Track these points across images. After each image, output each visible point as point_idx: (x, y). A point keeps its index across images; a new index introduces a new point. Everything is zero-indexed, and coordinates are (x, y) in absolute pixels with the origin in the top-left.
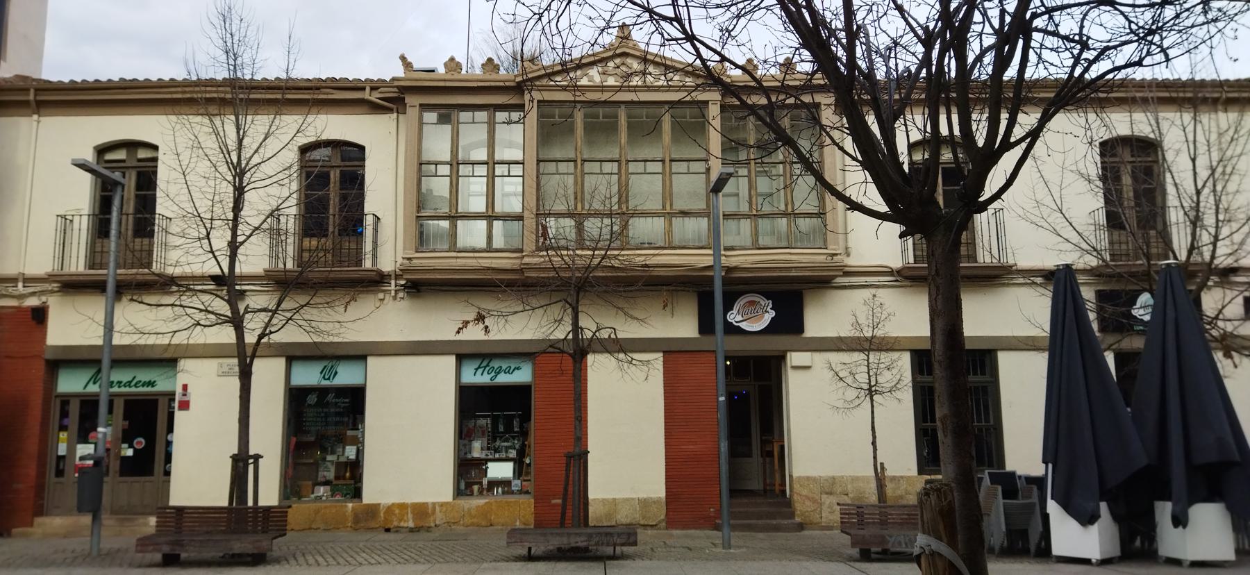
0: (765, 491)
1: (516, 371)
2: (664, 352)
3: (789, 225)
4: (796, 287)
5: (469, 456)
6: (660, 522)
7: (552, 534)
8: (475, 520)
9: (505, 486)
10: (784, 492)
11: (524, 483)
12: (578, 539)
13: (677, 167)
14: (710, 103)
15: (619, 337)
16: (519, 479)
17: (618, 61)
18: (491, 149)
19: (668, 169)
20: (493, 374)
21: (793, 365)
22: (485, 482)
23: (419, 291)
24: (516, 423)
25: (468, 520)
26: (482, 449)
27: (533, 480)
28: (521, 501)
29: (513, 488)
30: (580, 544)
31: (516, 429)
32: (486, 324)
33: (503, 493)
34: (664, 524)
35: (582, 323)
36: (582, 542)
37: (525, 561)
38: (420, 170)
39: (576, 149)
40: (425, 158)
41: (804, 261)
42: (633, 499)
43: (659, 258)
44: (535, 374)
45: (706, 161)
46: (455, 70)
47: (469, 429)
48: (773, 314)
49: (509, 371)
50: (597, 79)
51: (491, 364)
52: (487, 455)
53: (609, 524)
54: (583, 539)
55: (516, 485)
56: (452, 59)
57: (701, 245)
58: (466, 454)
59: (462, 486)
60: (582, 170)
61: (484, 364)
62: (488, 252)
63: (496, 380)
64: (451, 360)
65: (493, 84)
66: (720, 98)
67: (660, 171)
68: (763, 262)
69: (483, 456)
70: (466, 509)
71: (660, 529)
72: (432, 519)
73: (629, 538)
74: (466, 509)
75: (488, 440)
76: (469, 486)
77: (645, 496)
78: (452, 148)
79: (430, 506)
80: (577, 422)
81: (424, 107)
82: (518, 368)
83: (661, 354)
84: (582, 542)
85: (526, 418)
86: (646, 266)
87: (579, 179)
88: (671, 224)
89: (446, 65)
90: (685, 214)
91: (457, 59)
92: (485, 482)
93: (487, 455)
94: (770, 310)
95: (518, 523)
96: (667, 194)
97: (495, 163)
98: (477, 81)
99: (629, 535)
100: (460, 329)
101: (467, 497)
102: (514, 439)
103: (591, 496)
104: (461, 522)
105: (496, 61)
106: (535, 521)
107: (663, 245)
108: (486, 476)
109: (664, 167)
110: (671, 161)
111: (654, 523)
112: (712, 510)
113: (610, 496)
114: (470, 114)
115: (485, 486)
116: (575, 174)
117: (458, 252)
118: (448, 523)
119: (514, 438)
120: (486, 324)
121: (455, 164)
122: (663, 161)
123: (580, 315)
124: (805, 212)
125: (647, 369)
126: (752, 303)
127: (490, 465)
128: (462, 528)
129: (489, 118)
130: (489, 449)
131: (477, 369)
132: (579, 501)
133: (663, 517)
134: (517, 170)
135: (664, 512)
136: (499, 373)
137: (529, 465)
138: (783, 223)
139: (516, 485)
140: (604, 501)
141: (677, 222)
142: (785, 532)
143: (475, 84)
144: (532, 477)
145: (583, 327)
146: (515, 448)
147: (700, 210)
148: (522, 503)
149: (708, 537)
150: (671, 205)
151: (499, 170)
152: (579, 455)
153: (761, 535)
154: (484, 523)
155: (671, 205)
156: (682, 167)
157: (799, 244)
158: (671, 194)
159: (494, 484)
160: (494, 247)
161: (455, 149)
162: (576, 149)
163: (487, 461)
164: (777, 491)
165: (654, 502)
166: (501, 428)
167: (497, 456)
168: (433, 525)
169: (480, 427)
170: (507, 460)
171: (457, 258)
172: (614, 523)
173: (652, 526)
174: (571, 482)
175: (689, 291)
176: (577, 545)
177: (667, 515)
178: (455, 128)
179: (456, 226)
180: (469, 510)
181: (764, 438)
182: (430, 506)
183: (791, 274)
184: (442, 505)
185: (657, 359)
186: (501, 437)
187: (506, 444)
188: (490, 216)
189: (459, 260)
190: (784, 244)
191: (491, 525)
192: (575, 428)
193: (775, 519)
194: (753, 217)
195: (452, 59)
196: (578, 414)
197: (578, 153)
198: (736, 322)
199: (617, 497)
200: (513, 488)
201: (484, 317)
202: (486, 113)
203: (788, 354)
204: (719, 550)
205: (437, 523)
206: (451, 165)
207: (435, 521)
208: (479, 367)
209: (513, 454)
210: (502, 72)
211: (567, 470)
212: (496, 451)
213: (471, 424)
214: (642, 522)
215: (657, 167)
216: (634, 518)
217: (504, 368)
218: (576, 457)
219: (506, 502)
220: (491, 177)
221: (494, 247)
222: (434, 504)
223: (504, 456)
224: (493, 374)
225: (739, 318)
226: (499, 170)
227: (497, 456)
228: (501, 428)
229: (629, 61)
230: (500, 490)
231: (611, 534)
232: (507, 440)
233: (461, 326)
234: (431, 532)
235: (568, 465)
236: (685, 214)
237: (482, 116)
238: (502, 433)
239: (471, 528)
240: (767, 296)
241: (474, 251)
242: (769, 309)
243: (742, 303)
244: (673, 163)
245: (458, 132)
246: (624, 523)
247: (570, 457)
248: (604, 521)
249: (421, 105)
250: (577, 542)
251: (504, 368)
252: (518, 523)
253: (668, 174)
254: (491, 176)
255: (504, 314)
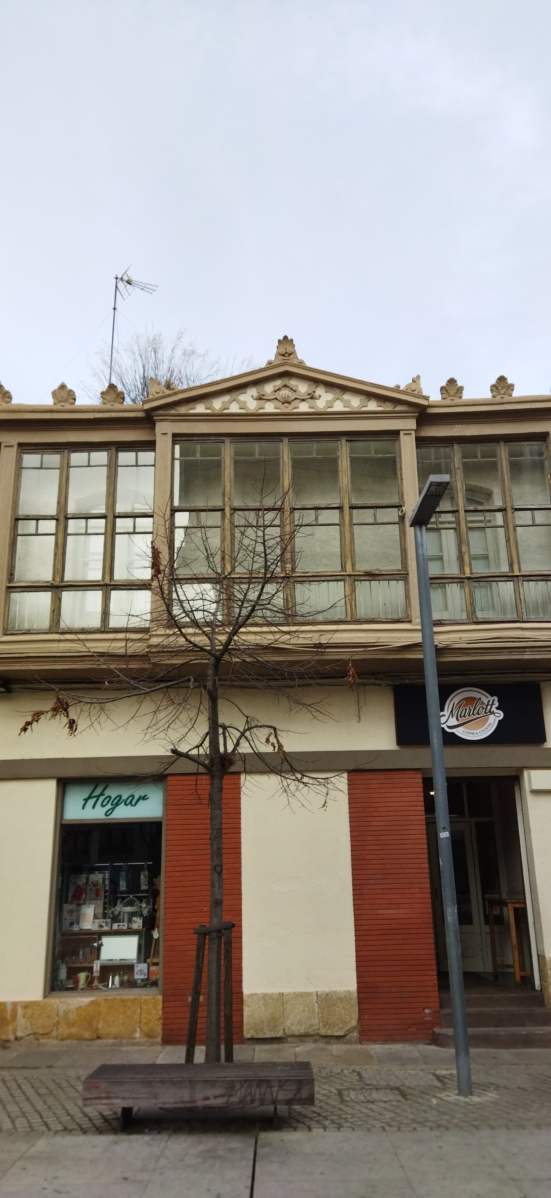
0: (496, 975)
1: (141, 801)
2: (350, 772)
3: (517, 591)
4: (529, 677)
5: (76, 928)
6: (350, 1031)
7: (162, 1082)
8: (74, 1030)
9: (124, 974)
10: (528, 980)
11: (153, 968)
12: (211, 1092)
13: (359, 516)
14: (402, 433)
15: (287, 749)
16: (145, 962)
17: (278, 383)
18: (111, 498)
19: (347, 518)
20: (109, 806)
21: (535, 787)
22: (96, 966)
23: (9, 691)
24: (143, 878)
25: (64, 1030)
26: (95, 917)
27: (161, 964)
28: (144, 997)
29: (137, 977)
30: (213, 1102)
31: (144, 887)
32: (72, 716)
33: (122, 984)
34: (356, 1034)
35: (222, 719)
36: (216, 1097)
37: (115, 1131)
38: (15, 527)
39: (224, 495)
40: (23, 511)
41: (542, 638)
42: (309, 994)
43: (337, 635)
44: (167, 805)
45: (399, 507)
46: (66, 401)
47: (79, 886)
48: (501, 715)
49: (131, 802)
50: (252, 405)
51: (107, 793)
52: (101, 926)
53: (273, 1035)
54: (217, 1092)
55: (141, 971)
56: (63, 387)
57: (395, 617)
58: (72, 924)
59: (63, 974)
60: (232, 523)
61: (97, 792)
62: (103, 632)
63: (112, 816)
64: (50, 787)
65: (114, 415)
66: (414, 427)
67: (337, 522)
68: (484, 640)
69: (96, 928)
70: (61, 1013)
71: (350, 1042)
72: (11, 1028)
73: (299, 1090)
74: (61, 1013)
75: (105, 904)
76: (73, 973)
77: (327, 990)
78: (59, 497)
79: (9, 1009)
80: (216, 876)
81: (25, 448)
82: (144, 798)
83: (345, 775)
84: (216, 1097)
85: (155, 872)
86: (319, 646)
87: (228, 534)
88: (353, 591)
89: (54, 394)
90: (372, 576)
91: (69, 387)
92: (96, 966)
93: (101, 926)
94: (496, 711)
95: (138, 1035)
96: (347, 552)
97: (116, 517)
98: (94, 411)
99: (300, 1084)
100: (28, 723)
101: (66, 993)
102: (141, 902)
103: (248, 988)
104: (54, 1033)
105: (120, 388)
106: (164, 1030)
107: (343, 617)
108: (98, 958)
109: (342, 517)
110: (352, 508)
111: (341, 1034)
112: (427, 1011)
113: (274, 990)
114: (85, 455)
115: (96, 974)
116: (222, 527)
117: (62, 633)
118: (35, 1034)
119: (140, 899)
120: (72, 716)
121: (62, 518)
122: (340, 508)
123: (220, 702)
124: (537, 573)
125: (324, 790)
126: (470, 700)
127: (105, 940)
128: (54, 1042)
129: (110, 459)
130: (105, 916)
131: (86, 800)
132: (218, 1013)
133: (354, 1023)
134: (145, 524)
135: (355, 1016)
136: (117, 805)
137: (158, 939)
138: (507, 588)
139: (141, 971)
140: (265, 996)
141: (362, 587)
142: (540, 1047)
143: (91, 416)
144: (160, 960)
145: (227, 724)
146: (141, 915)
147: (393, 570)
148: (146, 1002)
149: (426, 1060)
150: (353, 565)
151: (122, 524)
152: (219, 931)
153: (506, 1054)
154: (87, 1034)
155: (353, 565)
156: (367, 516)
157: (532, 617)
158: (352, 552)
159: (109, 970)
160: (110, 626)
161: (63, 500)
162: (224, 495)
163: (101, 934)
164: (518, 978)
165: (341, 999)
166: (123, 885)
167: (115, 926)
168: (11, 1037)
169: (94, 885)
170: (129, 932)
171: (59, 641)
172: (280, 1034)
173: (338, 1037)
174: (204, 980)
175: (380, 685)
176: (207, 1102)
177: (359, 1019)
178: (65, 474)
179: (60, 599)
180: (66, 1013)
181: (486, 896)
182: (9, 1009)
183: (526, 657)
184: (27, 1006)
185: (341, 782)
186: (123, 899)
187: (128, 909)
188: (106, 585)
189: (62, 645)
190: (514, 617)
191: (98, 1038)
192: (213, 885)
193: (523, 1025)
194: (466, 581)
195: (63, 387)
196: (216, 862)
197: (227, 500)
198: (449, 727)
199: (285, 991)
200: (137, 977)
201: (68, 706)
202: (106, 453)
203: (526, 773)
204: (452, 1096)
205: (19, 1034)
206: (57, 520)
207: (15, 1031)
208: (90, 797)
209: (138, 923)
210: (128, 401)
211: (200, 957)
212: (115, 919)
213: (82, 880)
214: (323, 1032)
215: (333, 516)
216: (311, 1025)
217: (124, 797)
218: (214, 934)
219: (122, 1001)
220: (111, 535)
221: (110, 626)
222: (15, 1004)
223: (125, 928)
224: (109, 806)
225: (453, 722)
226: (122, 524)
227: (115, 926)
228: (123, 885)
229: (293, 382)
230: (117, 978)
231: (268, 1083)
232: (131, 903)
233: (29, 719)
234: (9, 1048)
235: (200, 948)
236: (372, 576)
237: (101, 457)
238: (122, 892)
239: (69, 1042)
240: (490, 690)
241: (83, 631)
242: (494, 709)
243: (456, 700)
244: (354, 511)
245: (68, 478)
246: (296, 1033)
247: (203, 934)
248: (266, 1030)
249: (20, 445)
250: (207, 1099)
251: (124, 797)
252: (138, 1035)
253: (347, 525)
254: (109, 532)
255: (100, 701)
